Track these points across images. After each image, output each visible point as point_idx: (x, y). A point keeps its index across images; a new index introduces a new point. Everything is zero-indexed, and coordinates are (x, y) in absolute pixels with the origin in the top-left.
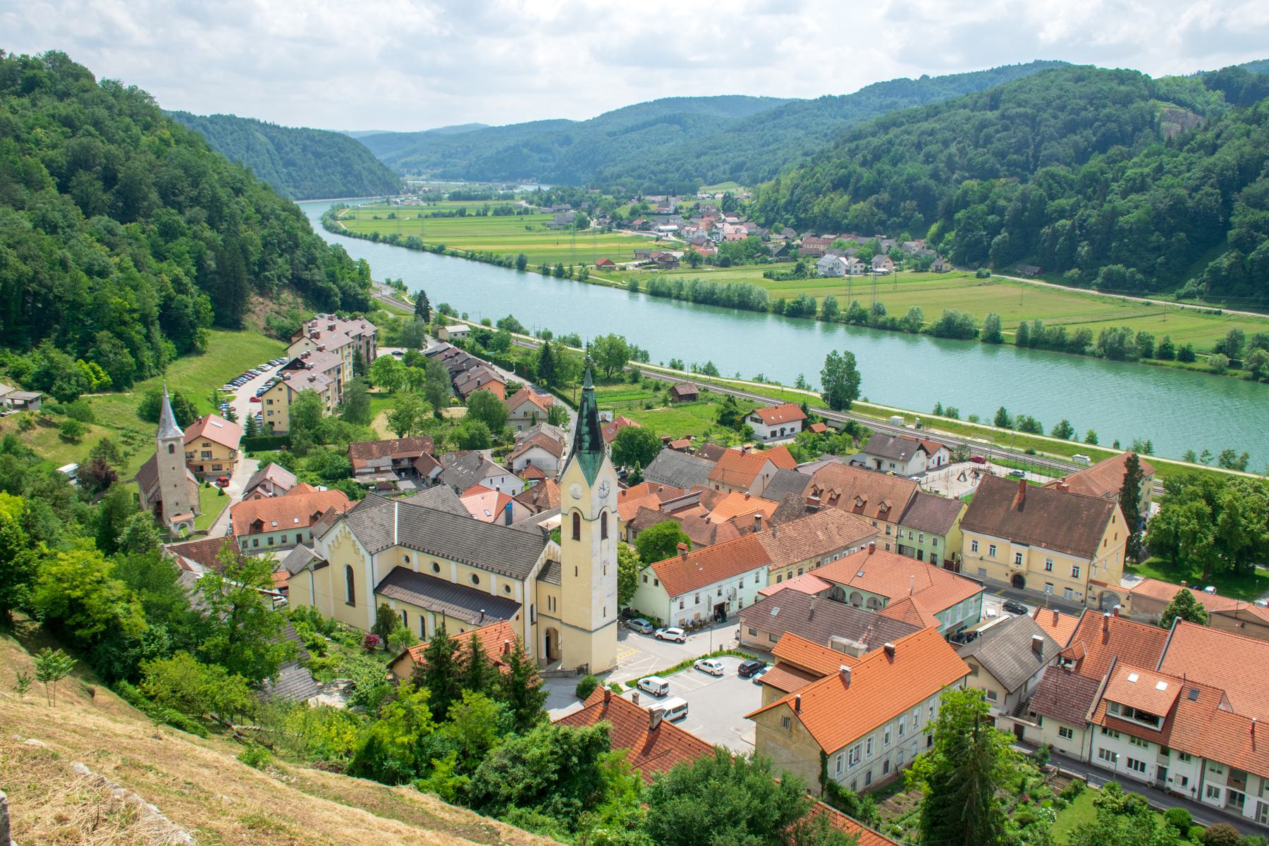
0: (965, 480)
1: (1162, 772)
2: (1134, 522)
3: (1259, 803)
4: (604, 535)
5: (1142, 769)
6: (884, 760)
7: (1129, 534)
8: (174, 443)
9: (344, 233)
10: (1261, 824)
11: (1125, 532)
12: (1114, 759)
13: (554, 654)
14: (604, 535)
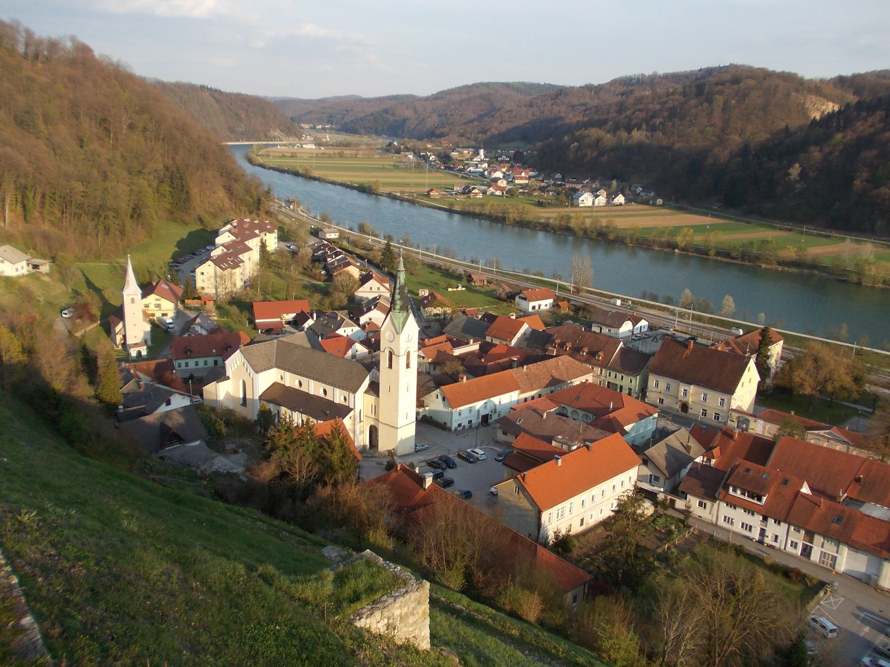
0: (657, 342)
1: (763, 532)
2: (763, 369)
3: (822, 552)
4: (408, 366)
5: (750, 530)
6: (581, 518)
7: (760, 380)
8: (134, 297)
9: (262, 166)
10: (821, 565)
11: (757, 378)
12: (732, 523)
13: (374, 443)
14: (408, 366)
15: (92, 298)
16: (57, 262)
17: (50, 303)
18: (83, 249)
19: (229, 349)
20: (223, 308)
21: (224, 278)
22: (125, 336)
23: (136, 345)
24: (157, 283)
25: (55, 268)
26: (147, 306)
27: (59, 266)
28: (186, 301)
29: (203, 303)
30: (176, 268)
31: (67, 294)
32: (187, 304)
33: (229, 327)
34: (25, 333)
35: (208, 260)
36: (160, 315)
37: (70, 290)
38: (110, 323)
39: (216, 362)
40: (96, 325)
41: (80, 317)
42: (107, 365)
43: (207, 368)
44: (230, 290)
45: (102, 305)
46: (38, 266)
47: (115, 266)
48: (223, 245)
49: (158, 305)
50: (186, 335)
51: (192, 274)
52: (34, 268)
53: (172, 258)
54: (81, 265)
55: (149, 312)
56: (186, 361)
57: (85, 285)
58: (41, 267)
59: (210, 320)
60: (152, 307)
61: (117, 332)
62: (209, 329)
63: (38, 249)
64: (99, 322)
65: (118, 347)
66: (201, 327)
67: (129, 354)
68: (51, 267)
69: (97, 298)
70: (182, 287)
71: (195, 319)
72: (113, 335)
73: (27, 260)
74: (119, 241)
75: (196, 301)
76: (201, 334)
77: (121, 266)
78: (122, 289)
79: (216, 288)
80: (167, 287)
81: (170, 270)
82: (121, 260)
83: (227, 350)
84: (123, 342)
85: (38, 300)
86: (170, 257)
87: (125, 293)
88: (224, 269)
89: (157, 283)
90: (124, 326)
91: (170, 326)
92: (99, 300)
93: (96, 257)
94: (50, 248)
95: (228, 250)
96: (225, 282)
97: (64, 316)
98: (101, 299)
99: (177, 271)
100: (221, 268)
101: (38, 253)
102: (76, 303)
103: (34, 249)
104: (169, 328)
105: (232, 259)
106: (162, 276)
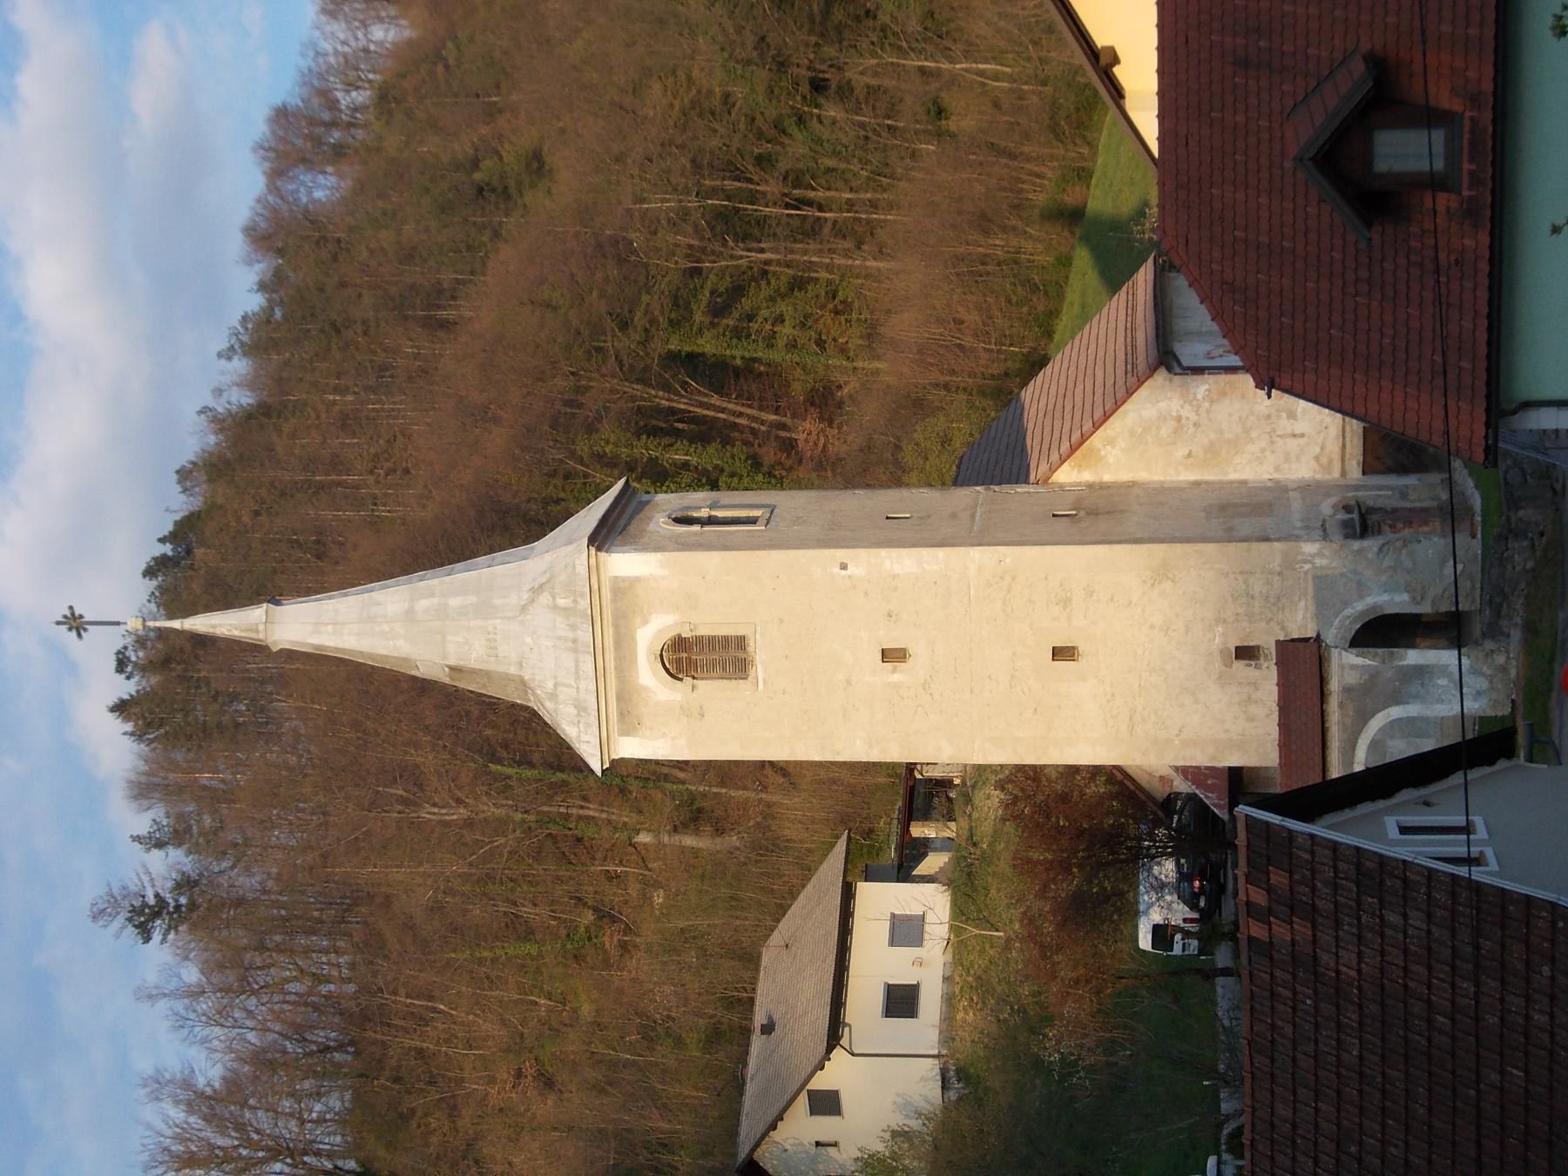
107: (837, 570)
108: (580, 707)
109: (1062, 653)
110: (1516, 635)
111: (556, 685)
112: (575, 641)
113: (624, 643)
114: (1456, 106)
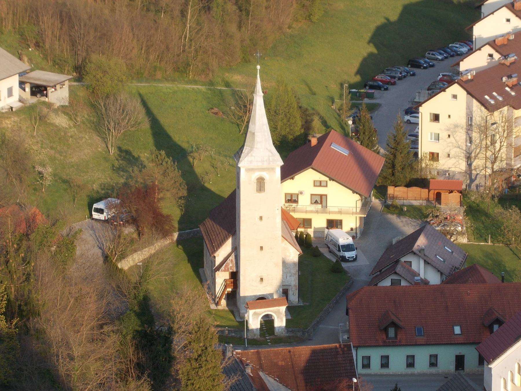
15: (165, 174)
16: (88, 80)
17: (65, 181)
18: (148, 48)
19: (496, 327)
20: (487, 215)
21: (490, 133)
22: (235, 276)
23: (261, 299)
24: (321, 141)
25: (82, 93)
26: (292, 199)
27: (93, 91)
28: (391, 190)
29: (432, 196)
30: (366, 100)
31: (106, 159)
32: (393, 198)
33: (498, 265)
34: (13, 264)
35: (451, 83)
36: (324, 224)
37: (113, 151)
38: (202, 238)
39: (460, 361)
40: (167, 242)
41: (134, 221)
42: (196, 355)
43: (438, 375)
44: (504, 165)
45: (185, 193)
46: (45, 88)
47: (220, 92)
48: (492, 43)
49: (321, 196)
50: (387, 283)
51: (407, 118)
52: (33, 93)
53: (359, 72)
54: (143, 87)
55: (296, 215)
56: (385, 351)
57: (150, 140)
58: (50, 90)
59: (452, 245)
60: (304, 201)
61: (217, 263)
62: (446, 271)
63: (47, 46)
64: (176, 235)
65: (217, 304)
66: (426, 263)
67: (243, 324)
68: (72, 91)
69: (175, 173)
70: (382, 151)
71: (415, 236)
72: (207, 270)
73: (21, 74)
74: (233, 28)
75: (415, 191)
76: (426, 282)
77: (234, 93)
78: (238, 154)
79: (469, 158)
80: (344, 152)
81: (353, 106)
82: (236, 78)
83: (492, 331)
84: (229, 290)
85: (40, 173)
86: (355, 70)
87: (244, 164)
88: (490, 108)
89: (321, 141)
90: (236, 249)
91: (348, 254)
92: (181, 180)
93: (177, 69)
94: (73, 44)
95: (506, 57)
96: (493, 143)
97: (96, 215)
98: (183, 175)
99: (372, 108)
100: (484, 103)
101: (46, 58)
102: (126, 185)
103: (37, 45)
104: (344, 259)
105: (514, 80)
106: (333, 122)
107: (277, 208)
108: (251, 162)
109: (261, 248)
110: (288, 335)
111: (254, 156)
112: (264, 161)
113: (263, 169)
114: (398, 339)
